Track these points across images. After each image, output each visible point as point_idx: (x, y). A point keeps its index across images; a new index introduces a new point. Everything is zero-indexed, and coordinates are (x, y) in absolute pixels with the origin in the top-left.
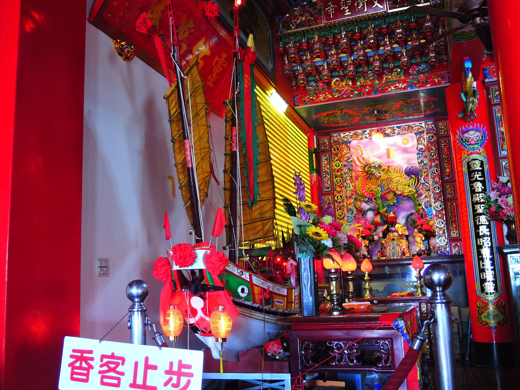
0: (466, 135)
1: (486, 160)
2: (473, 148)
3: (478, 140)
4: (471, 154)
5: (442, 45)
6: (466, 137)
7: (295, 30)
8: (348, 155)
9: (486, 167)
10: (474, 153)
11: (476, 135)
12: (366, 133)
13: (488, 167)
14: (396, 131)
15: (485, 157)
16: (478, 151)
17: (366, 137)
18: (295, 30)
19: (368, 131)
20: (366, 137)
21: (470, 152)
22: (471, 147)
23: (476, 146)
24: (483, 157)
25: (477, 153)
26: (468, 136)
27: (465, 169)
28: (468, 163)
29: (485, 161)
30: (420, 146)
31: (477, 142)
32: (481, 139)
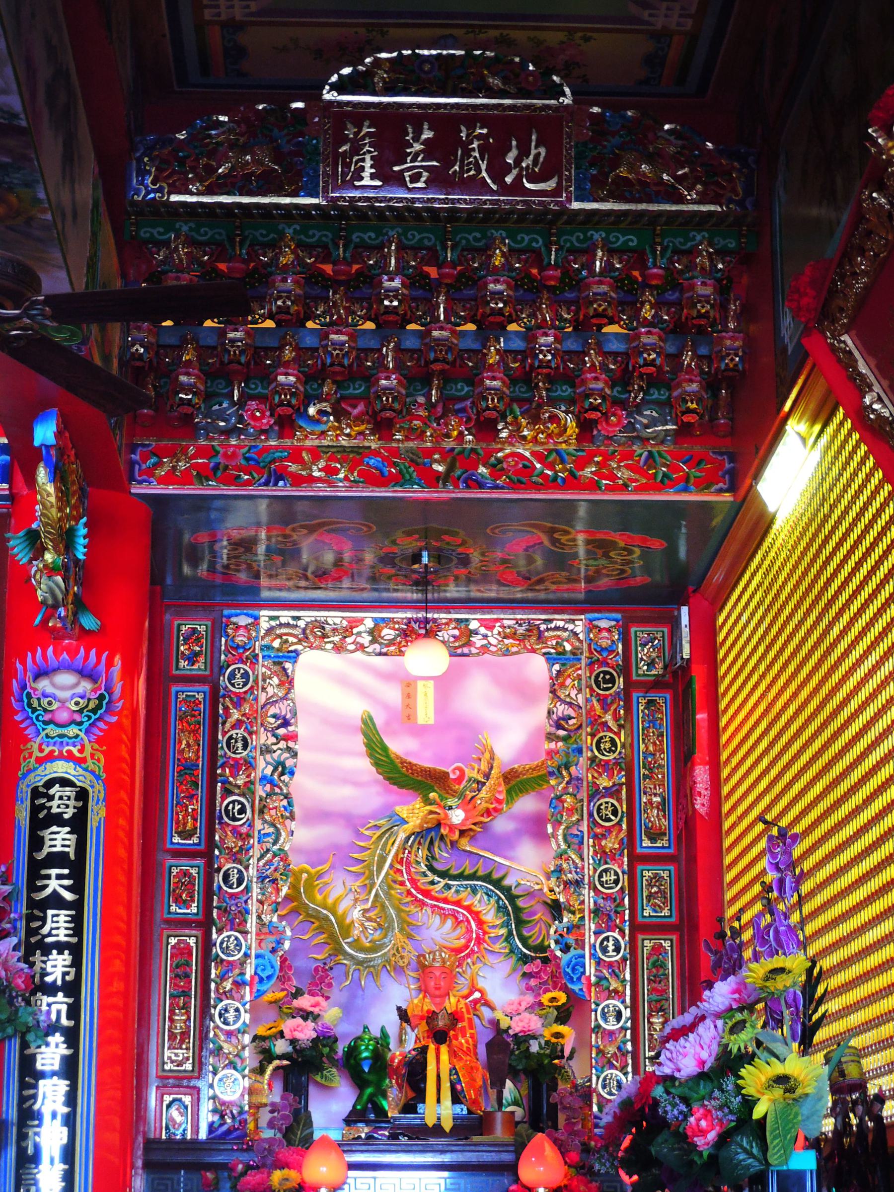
0: (44, 685)
1: (100, 787)
2: (61, 736)
3: (81, 711)
4: (50, 758)
5: (694, 411)
6: (45, 696)
7: (695, 208)
8: (282, 708)
9: (97, 815)
10: (61, 757)
11: (79, 690)
12: (361, 628)
13: (103, 813)
14: (478, 641)
15: (98, 777)
16: (75, 751)
17: (361, 647)
18: (695, 208)
19: (369, 624)
20: (361, 647)
21: (47, 750)
22: (52, 730)
23: (72, 730)
24: (89, 777)
25: (70, 757)
26: (49, 690)
27: (23, 814)
28: (36, 793)
29: (97, 792)
30: (561, 709)
31: (77, 717)
32: (92, 705)
